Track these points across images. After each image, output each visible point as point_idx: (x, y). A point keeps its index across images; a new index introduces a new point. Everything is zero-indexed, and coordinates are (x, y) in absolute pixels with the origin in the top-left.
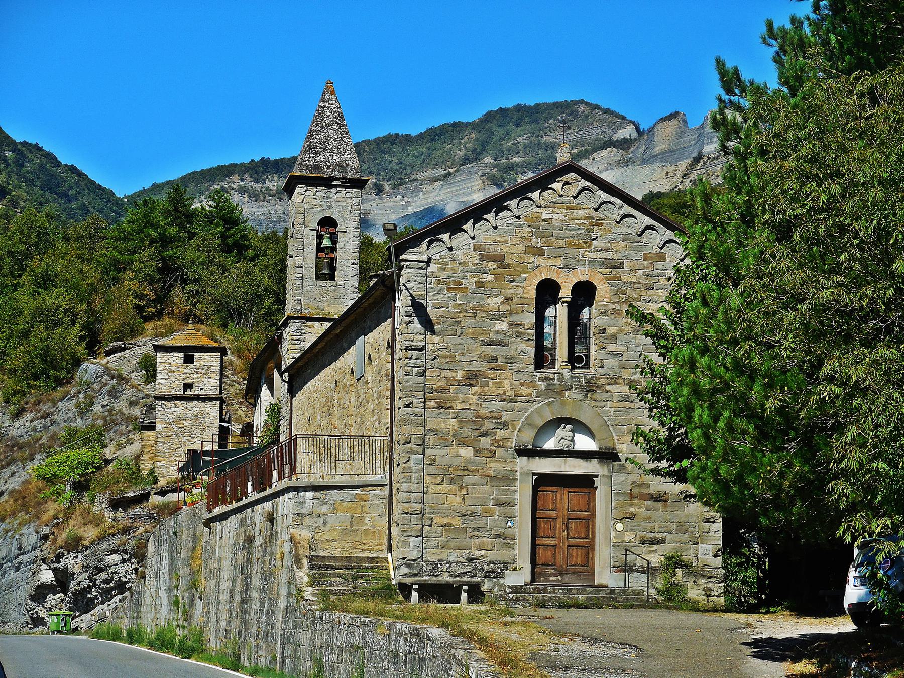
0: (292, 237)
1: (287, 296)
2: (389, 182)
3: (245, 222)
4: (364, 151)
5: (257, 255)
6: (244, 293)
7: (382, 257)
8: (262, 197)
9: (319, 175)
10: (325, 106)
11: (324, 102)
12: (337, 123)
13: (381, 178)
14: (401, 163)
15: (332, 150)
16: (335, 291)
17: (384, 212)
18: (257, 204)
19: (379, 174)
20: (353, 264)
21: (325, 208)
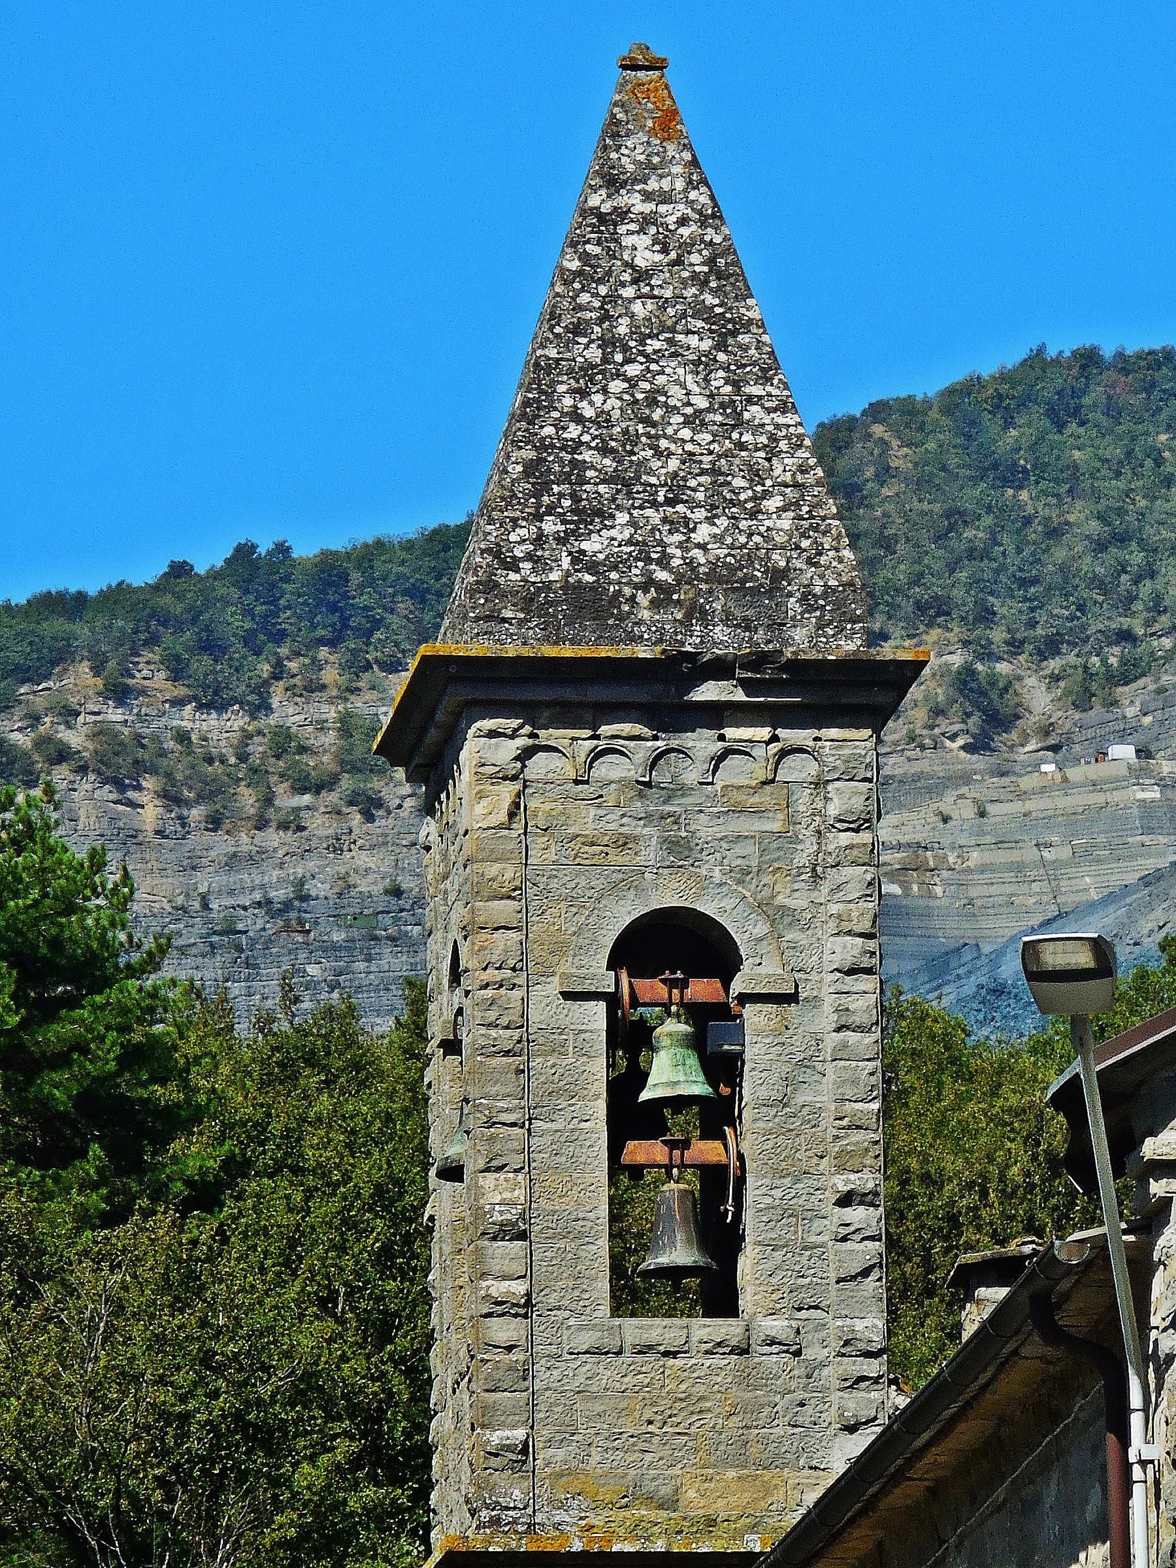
0: (452, 1047)
1: (440, 1427)
2: (1054, 664)
3: (152, 962)
4: (885, 473)
5: (236, 1167)
6: (165, 1416)
7: (1031, 1140)
8: (247, 799)
9: (604, 652)
10: (622, 214)
11: (613, 182)
12: (703, 311)
13: (998, 635)
14: (1121, 539)
15: (677, 493)
16: (746, 1380)
17: (1030, 854)
18: (221, 844)
19: (986, 616)
20: (845, 1200)
21: (650, 853)
